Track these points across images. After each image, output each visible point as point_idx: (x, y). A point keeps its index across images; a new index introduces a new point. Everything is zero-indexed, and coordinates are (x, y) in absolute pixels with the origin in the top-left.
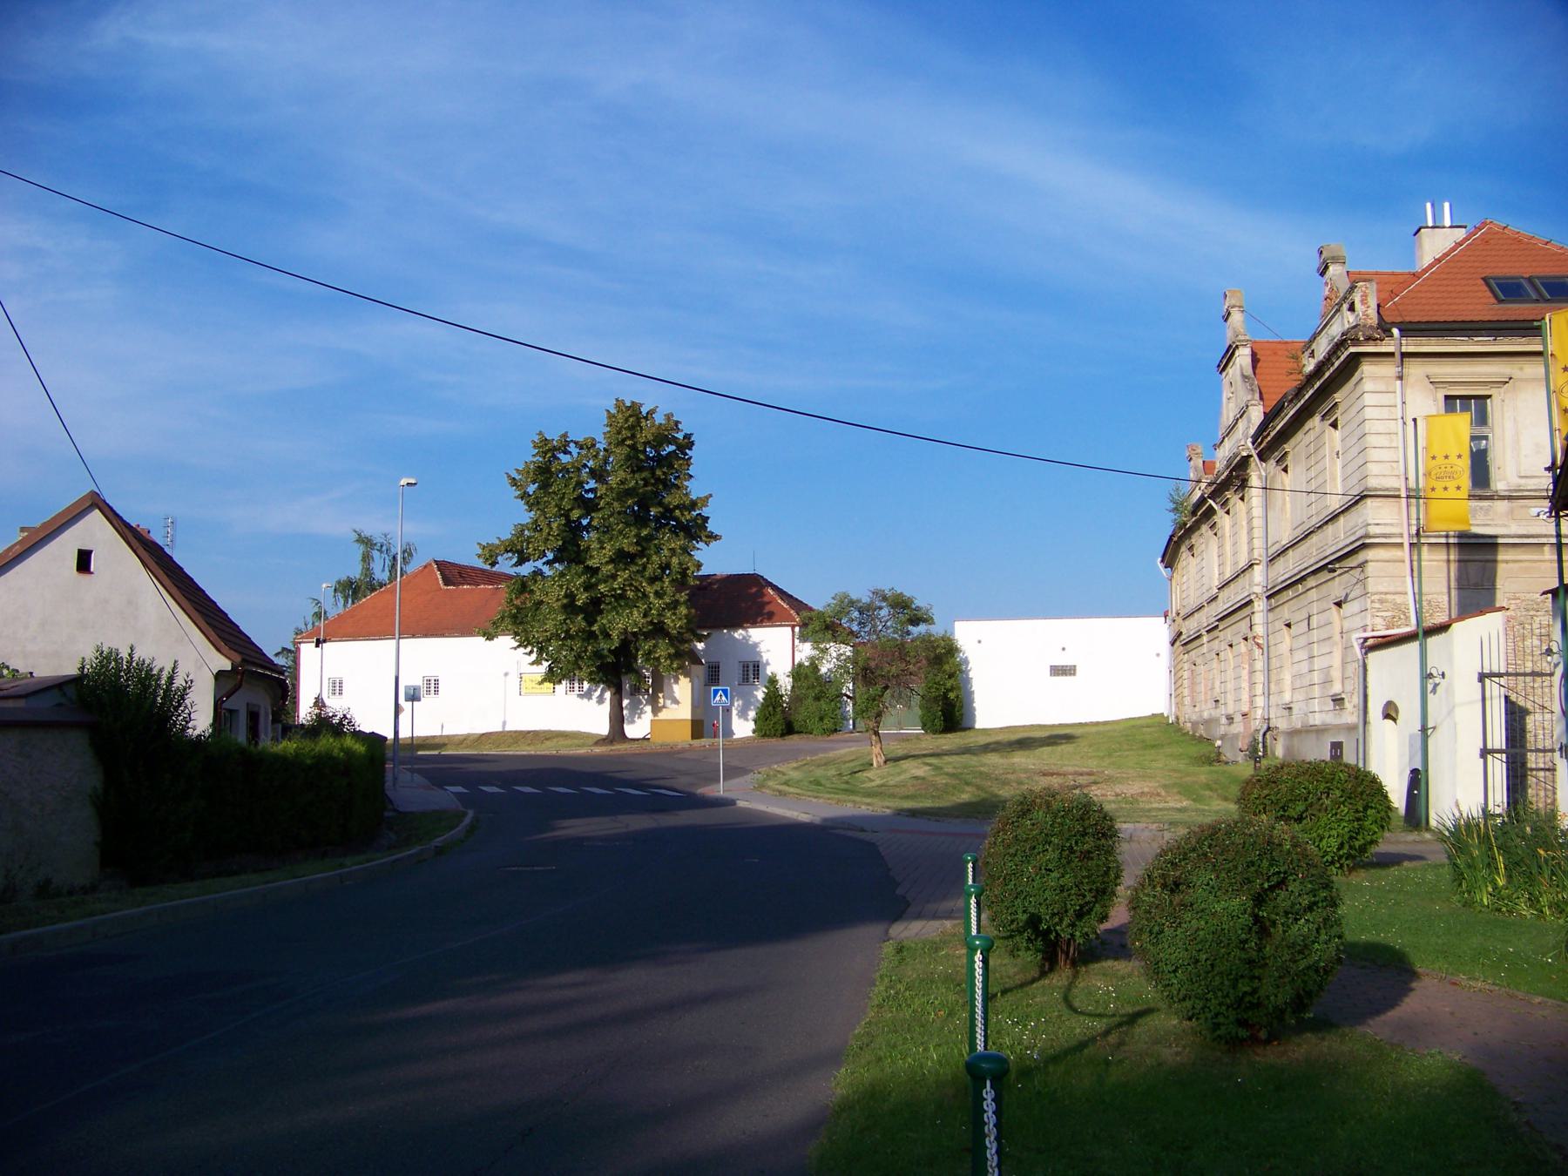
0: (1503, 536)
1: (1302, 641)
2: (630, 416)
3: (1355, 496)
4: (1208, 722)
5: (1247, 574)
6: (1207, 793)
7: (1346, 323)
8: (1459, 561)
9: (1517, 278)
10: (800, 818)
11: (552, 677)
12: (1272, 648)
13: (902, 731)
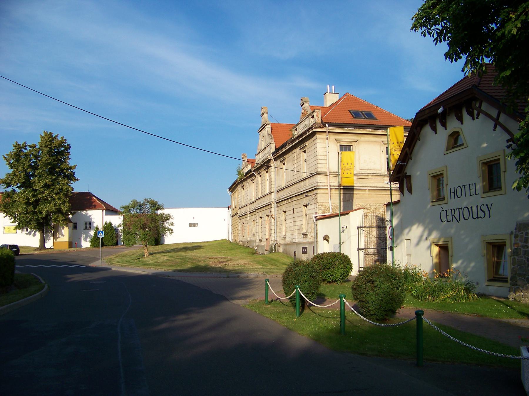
0: (356, 187)
1: (290, 217)
2: (50, 137)
3: (313, 174)
4: (249, 242)
5: (269, 196)
6: (265, 263)
7: (310, 121)
8: (343, 194)
9: (357, 111)
10: (142, 273)
11: (18, 227)
12: (278, 219)
13: (140, 245)
